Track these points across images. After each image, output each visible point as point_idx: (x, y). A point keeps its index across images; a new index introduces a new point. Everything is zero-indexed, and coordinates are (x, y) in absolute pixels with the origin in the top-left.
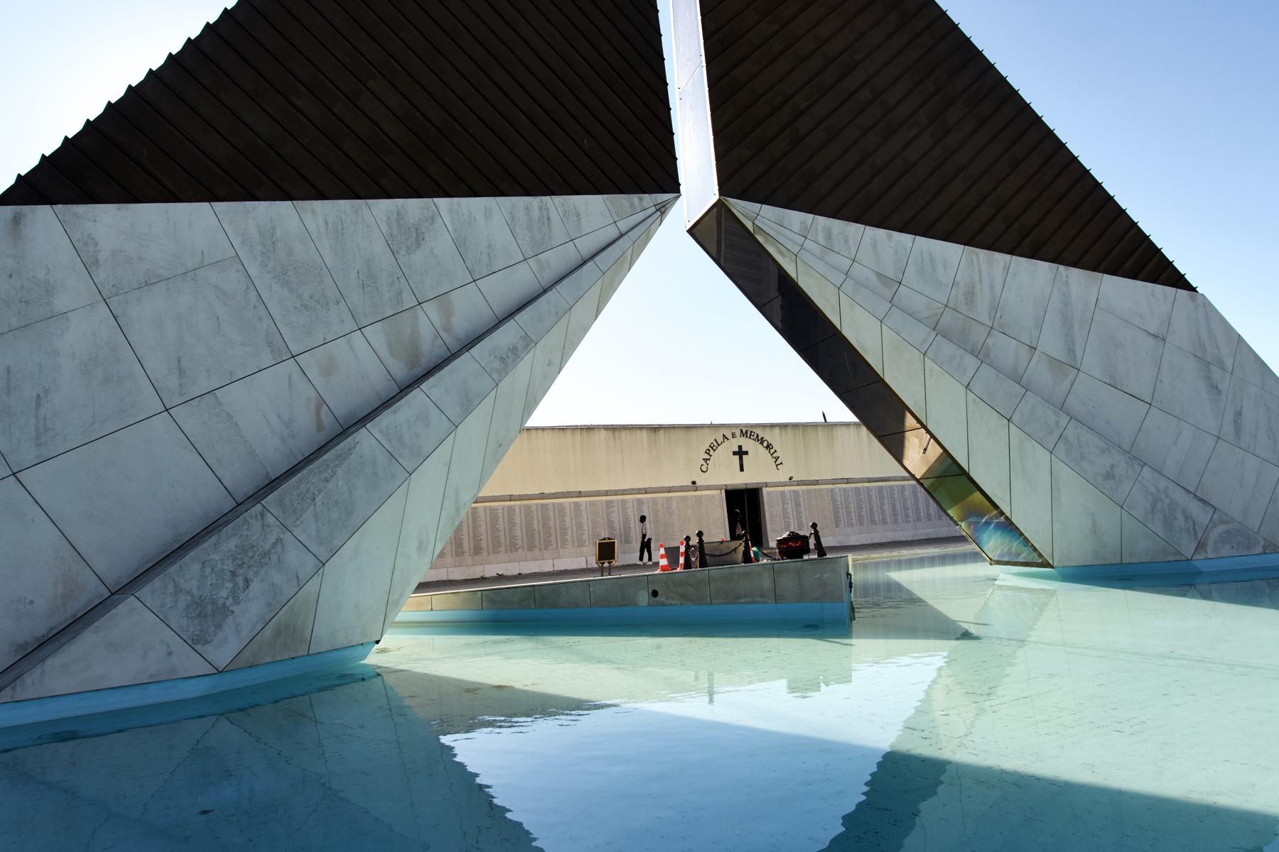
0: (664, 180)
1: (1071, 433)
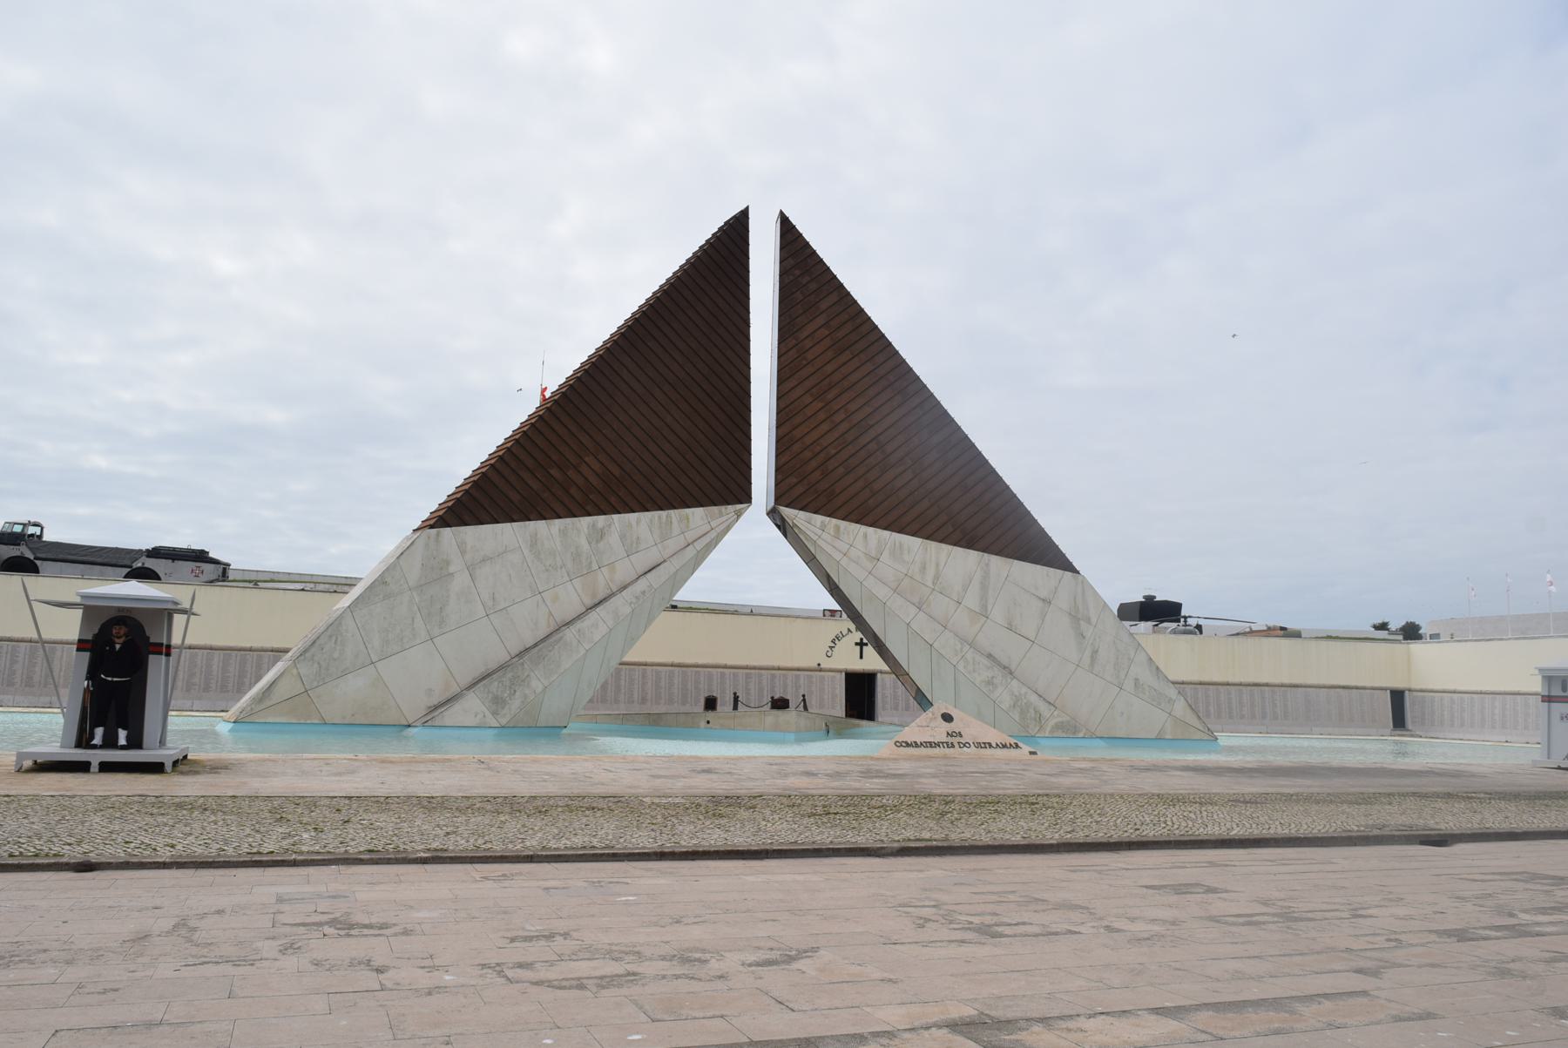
0: (742, 495)
1: (969, 656)
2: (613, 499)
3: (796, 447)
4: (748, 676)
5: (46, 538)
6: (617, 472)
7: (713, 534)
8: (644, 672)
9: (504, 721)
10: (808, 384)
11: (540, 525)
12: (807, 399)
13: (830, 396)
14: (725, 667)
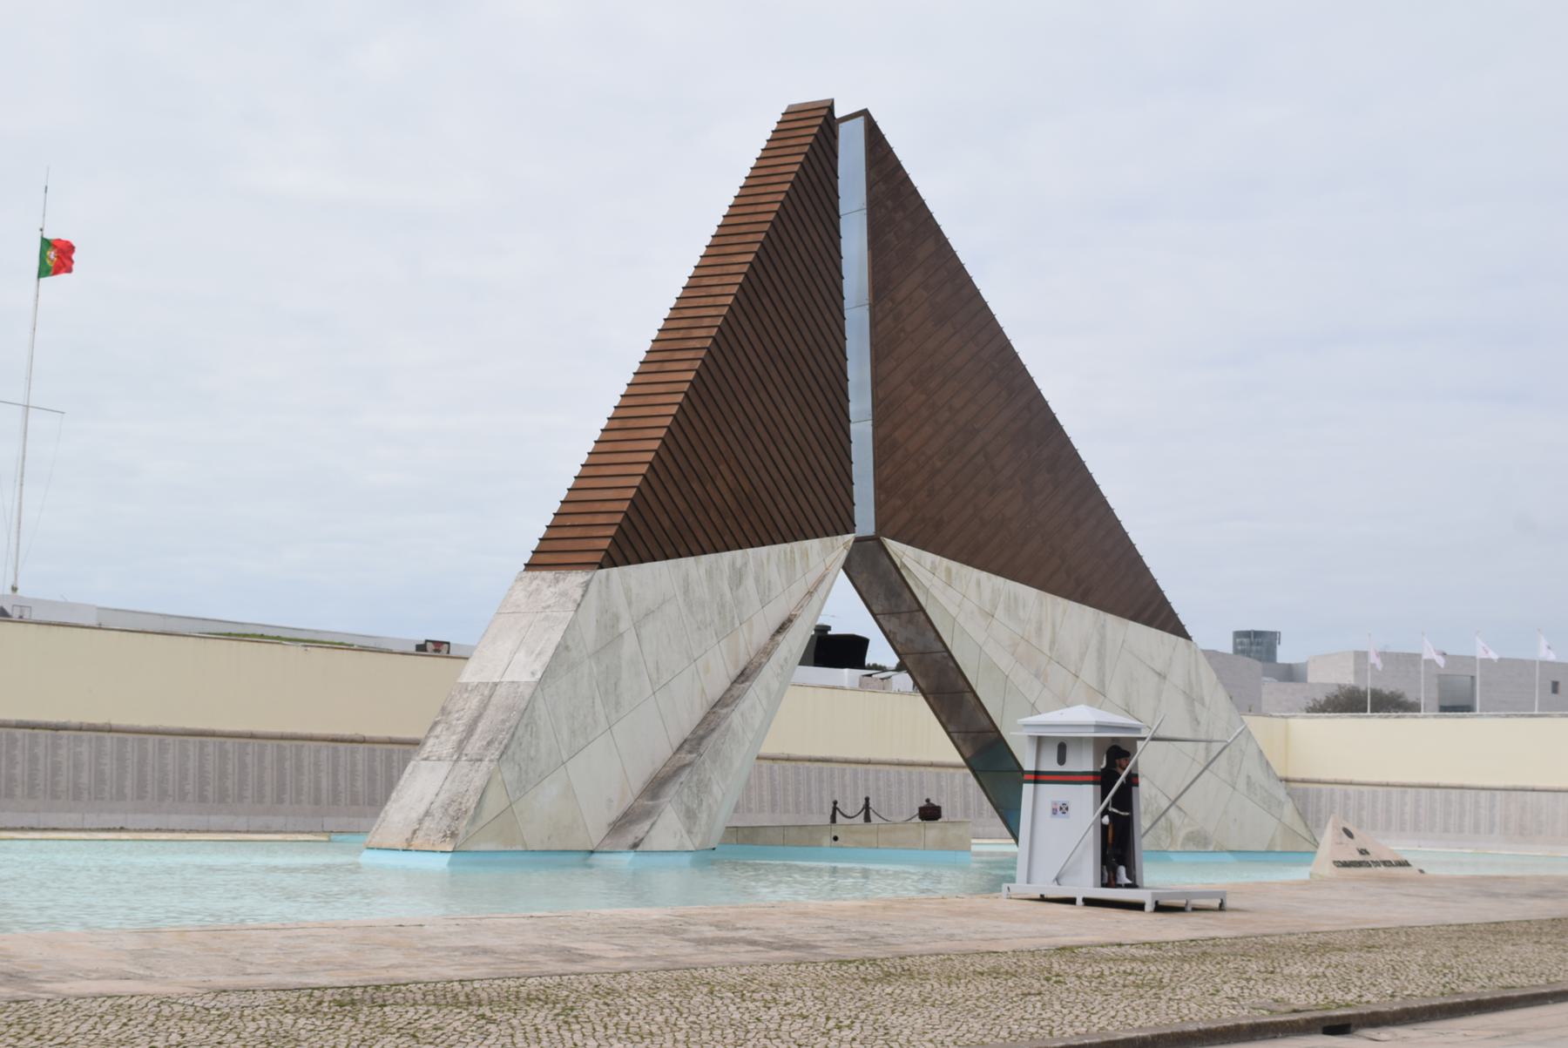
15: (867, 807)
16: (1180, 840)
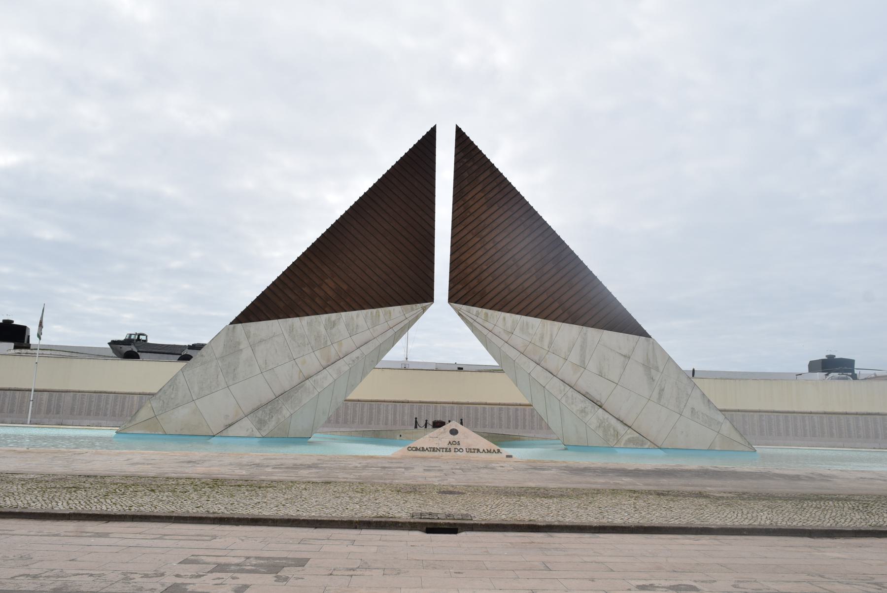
0: (426, 296)
2: (342, 304)
3: (462, 267)
4: (500, 410)
5: (149, 341)
6: (345, 287)
7: (406, 322)
8: (436, 407)
9: (264, 434)
10: (470, 227)
11: (296, 320)
12: (470, 236)
13: (484, 233)
14: (486, 404)
15: (416, 422)
16: (623, 442)
